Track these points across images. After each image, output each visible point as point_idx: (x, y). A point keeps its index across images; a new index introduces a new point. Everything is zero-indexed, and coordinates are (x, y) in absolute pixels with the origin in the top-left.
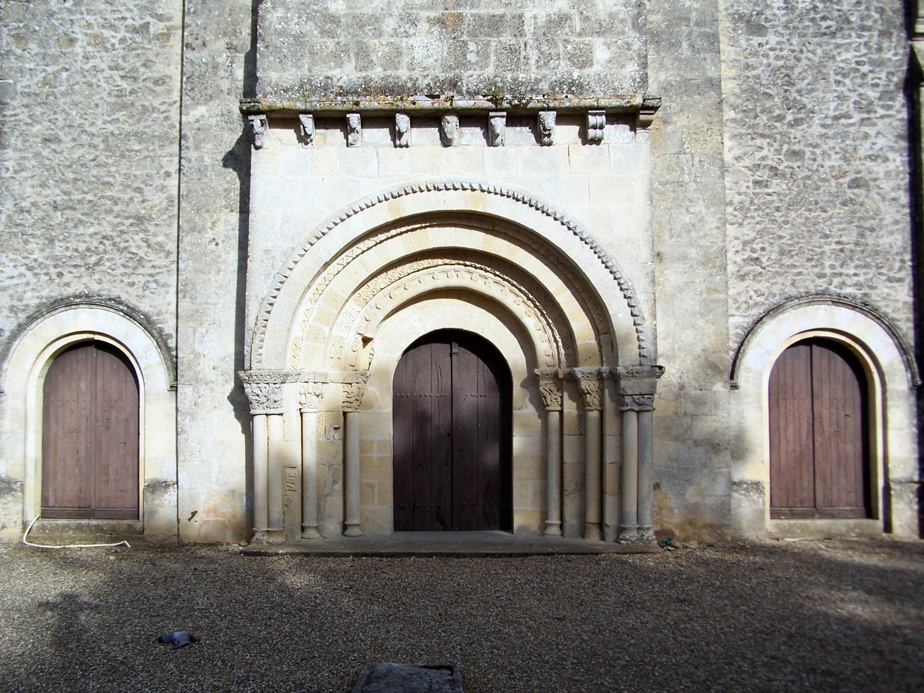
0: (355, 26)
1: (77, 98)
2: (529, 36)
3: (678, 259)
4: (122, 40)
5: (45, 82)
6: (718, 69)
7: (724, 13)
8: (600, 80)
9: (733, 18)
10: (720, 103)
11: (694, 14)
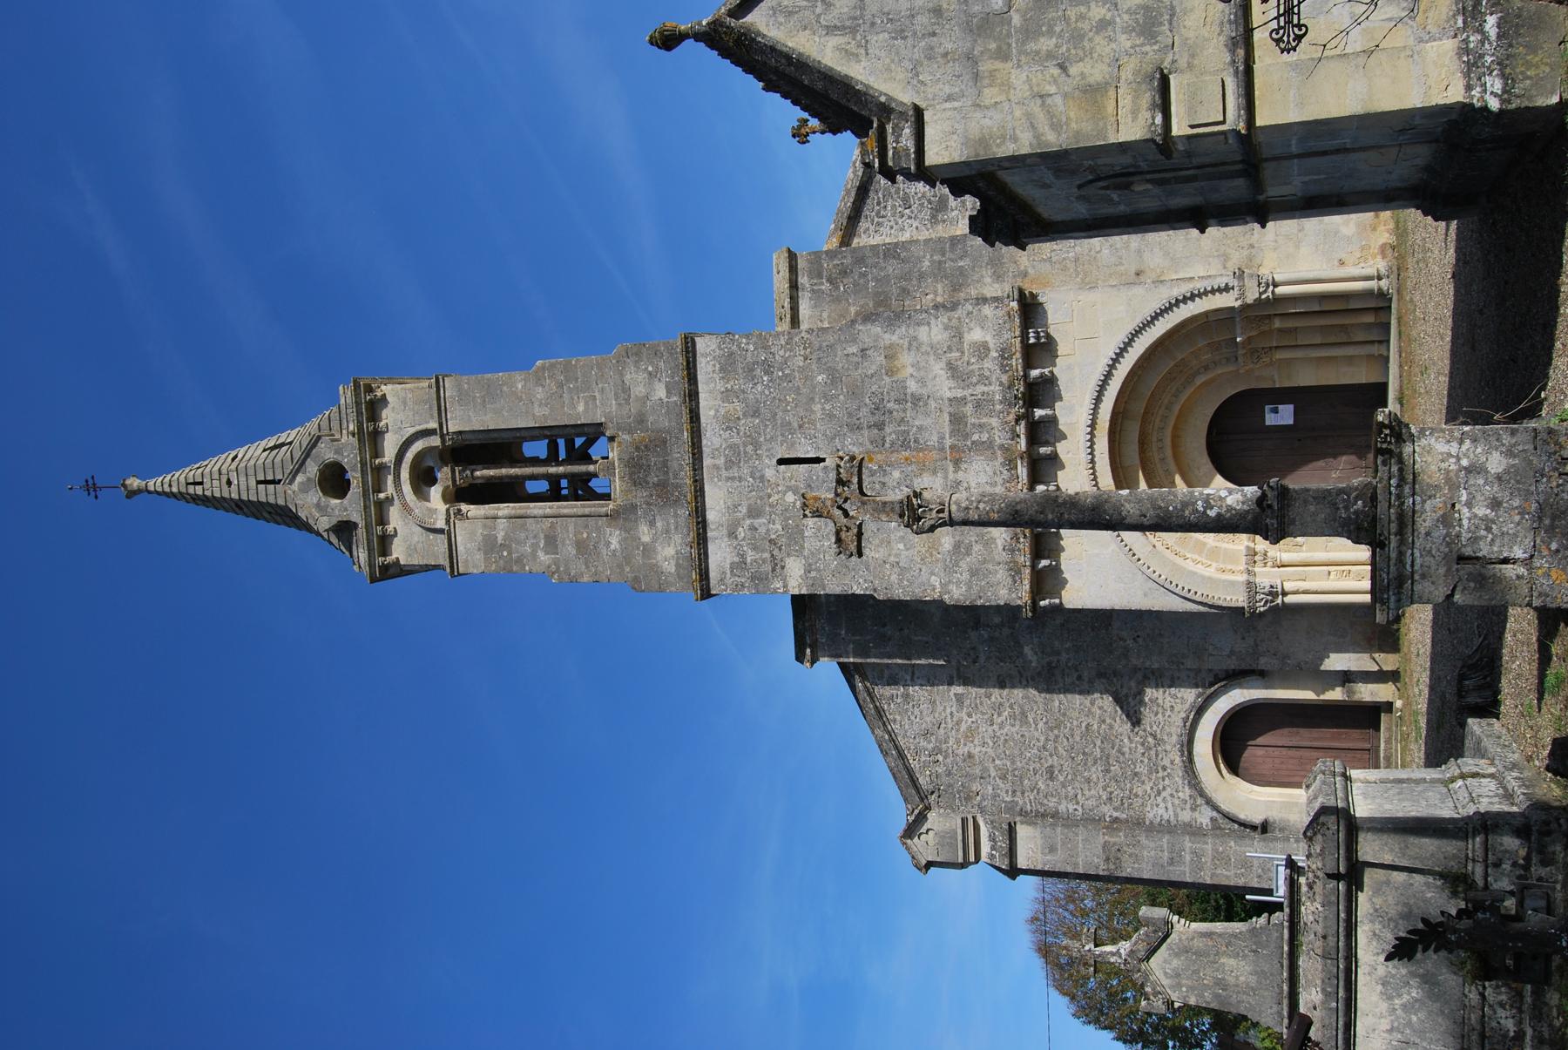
1: (1016, 752)
4: (970, 715)
5: (1003, 777)
8: (998, 334)
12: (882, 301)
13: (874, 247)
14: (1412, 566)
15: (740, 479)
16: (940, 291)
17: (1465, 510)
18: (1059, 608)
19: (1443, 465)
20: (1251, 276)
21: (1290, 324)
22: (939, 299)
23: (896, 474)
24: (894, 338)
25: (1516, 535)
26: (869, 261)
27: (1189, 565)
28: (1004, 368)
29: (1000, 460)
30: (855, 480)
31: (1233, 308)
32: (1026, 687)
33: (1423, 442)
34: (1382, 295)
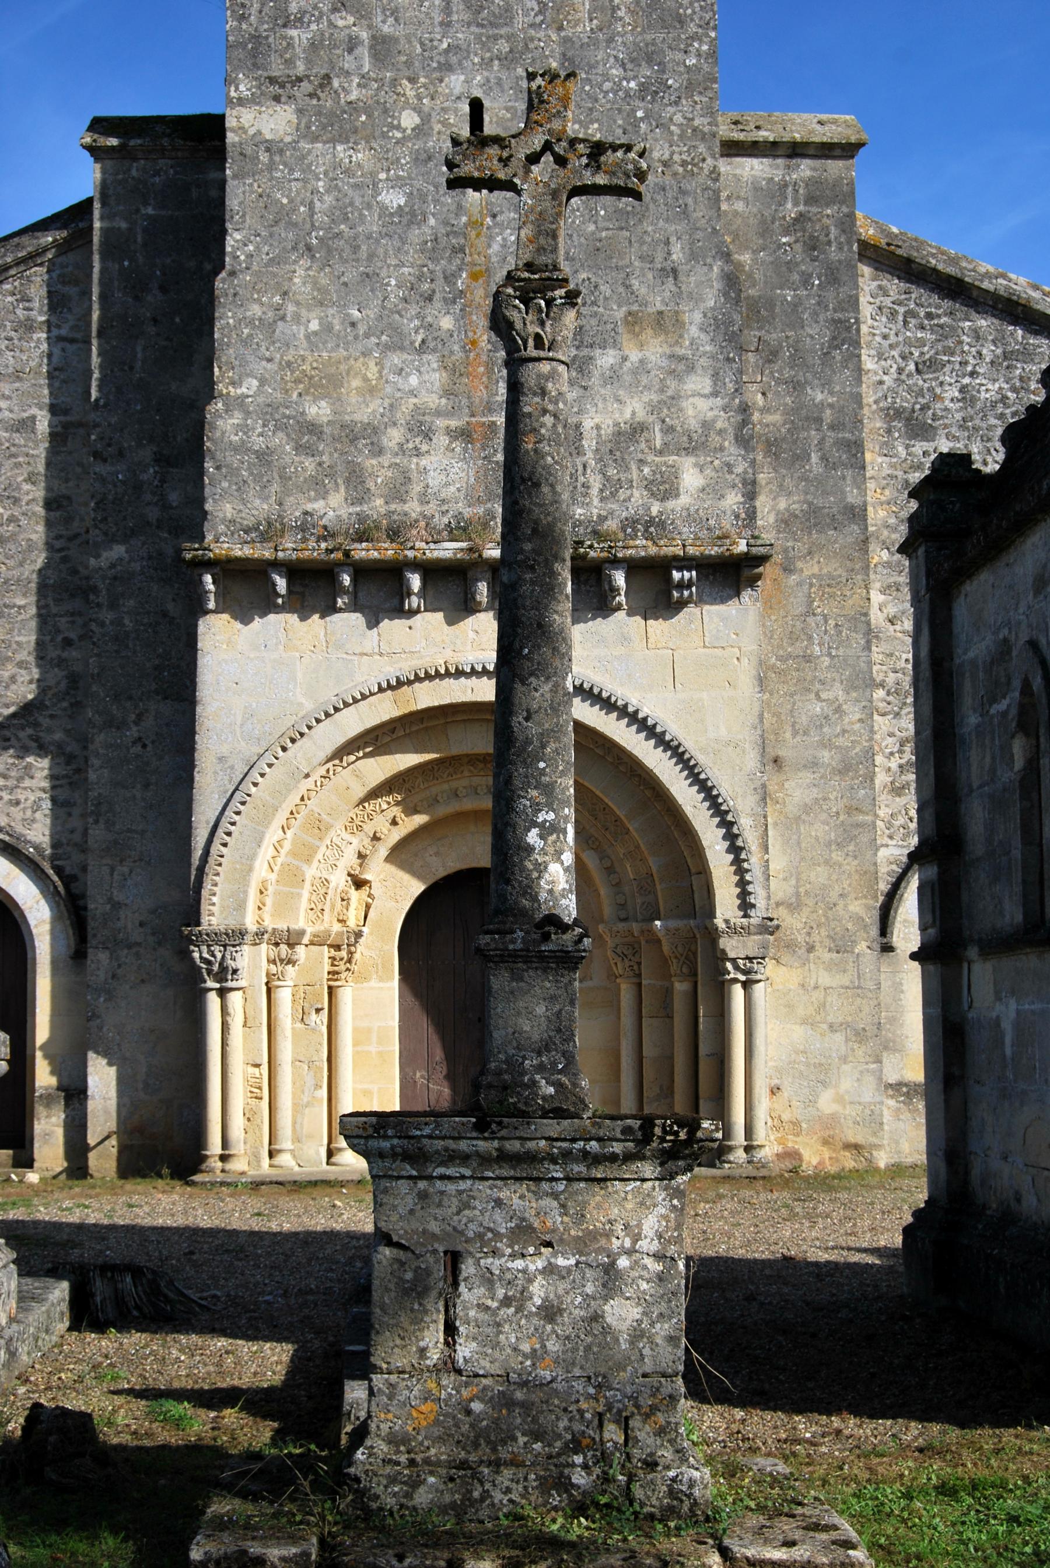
0: (344, 439)
2: (590, 455)
3: (805, 766)
6: (863, 492)
7: (874, 407)
8: (690, 517)
9: (887, 415)
10: (866, 541)
11: (828, 412)
12: (758, 312)
13: (854, 303)
14: (442, 1177)
15: (446, 25)
16: (769, 418)
17: (540, 1264)
18: (197, 609)
19: (619, 1227)
20: (765, 946)
21: (679, 1006)
22: (756, 417)
23: (447, 323)
24: (694, 331)
25: (495, 1346)
26: (830, 295)
27: (273, 834)
28: (629, 523)
29: (468, 512)
30: (601, 180)
31: (712, 914)
32: (49, 546)
33: (660, 1196)
34: (719, 1153)
